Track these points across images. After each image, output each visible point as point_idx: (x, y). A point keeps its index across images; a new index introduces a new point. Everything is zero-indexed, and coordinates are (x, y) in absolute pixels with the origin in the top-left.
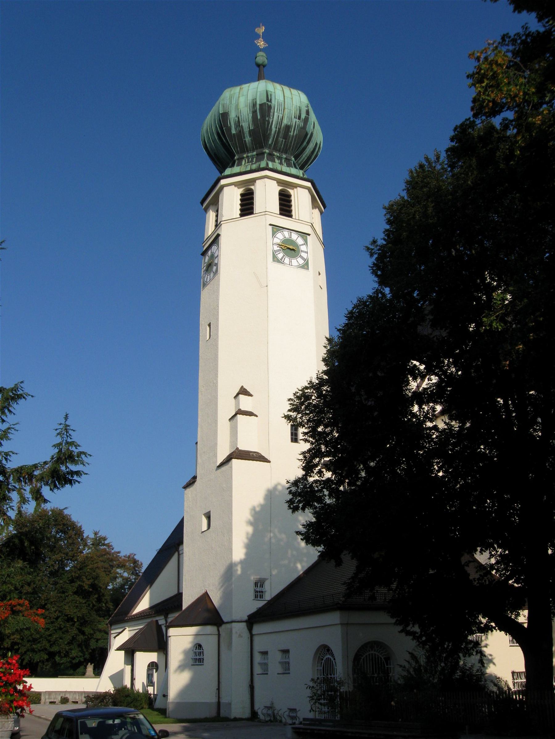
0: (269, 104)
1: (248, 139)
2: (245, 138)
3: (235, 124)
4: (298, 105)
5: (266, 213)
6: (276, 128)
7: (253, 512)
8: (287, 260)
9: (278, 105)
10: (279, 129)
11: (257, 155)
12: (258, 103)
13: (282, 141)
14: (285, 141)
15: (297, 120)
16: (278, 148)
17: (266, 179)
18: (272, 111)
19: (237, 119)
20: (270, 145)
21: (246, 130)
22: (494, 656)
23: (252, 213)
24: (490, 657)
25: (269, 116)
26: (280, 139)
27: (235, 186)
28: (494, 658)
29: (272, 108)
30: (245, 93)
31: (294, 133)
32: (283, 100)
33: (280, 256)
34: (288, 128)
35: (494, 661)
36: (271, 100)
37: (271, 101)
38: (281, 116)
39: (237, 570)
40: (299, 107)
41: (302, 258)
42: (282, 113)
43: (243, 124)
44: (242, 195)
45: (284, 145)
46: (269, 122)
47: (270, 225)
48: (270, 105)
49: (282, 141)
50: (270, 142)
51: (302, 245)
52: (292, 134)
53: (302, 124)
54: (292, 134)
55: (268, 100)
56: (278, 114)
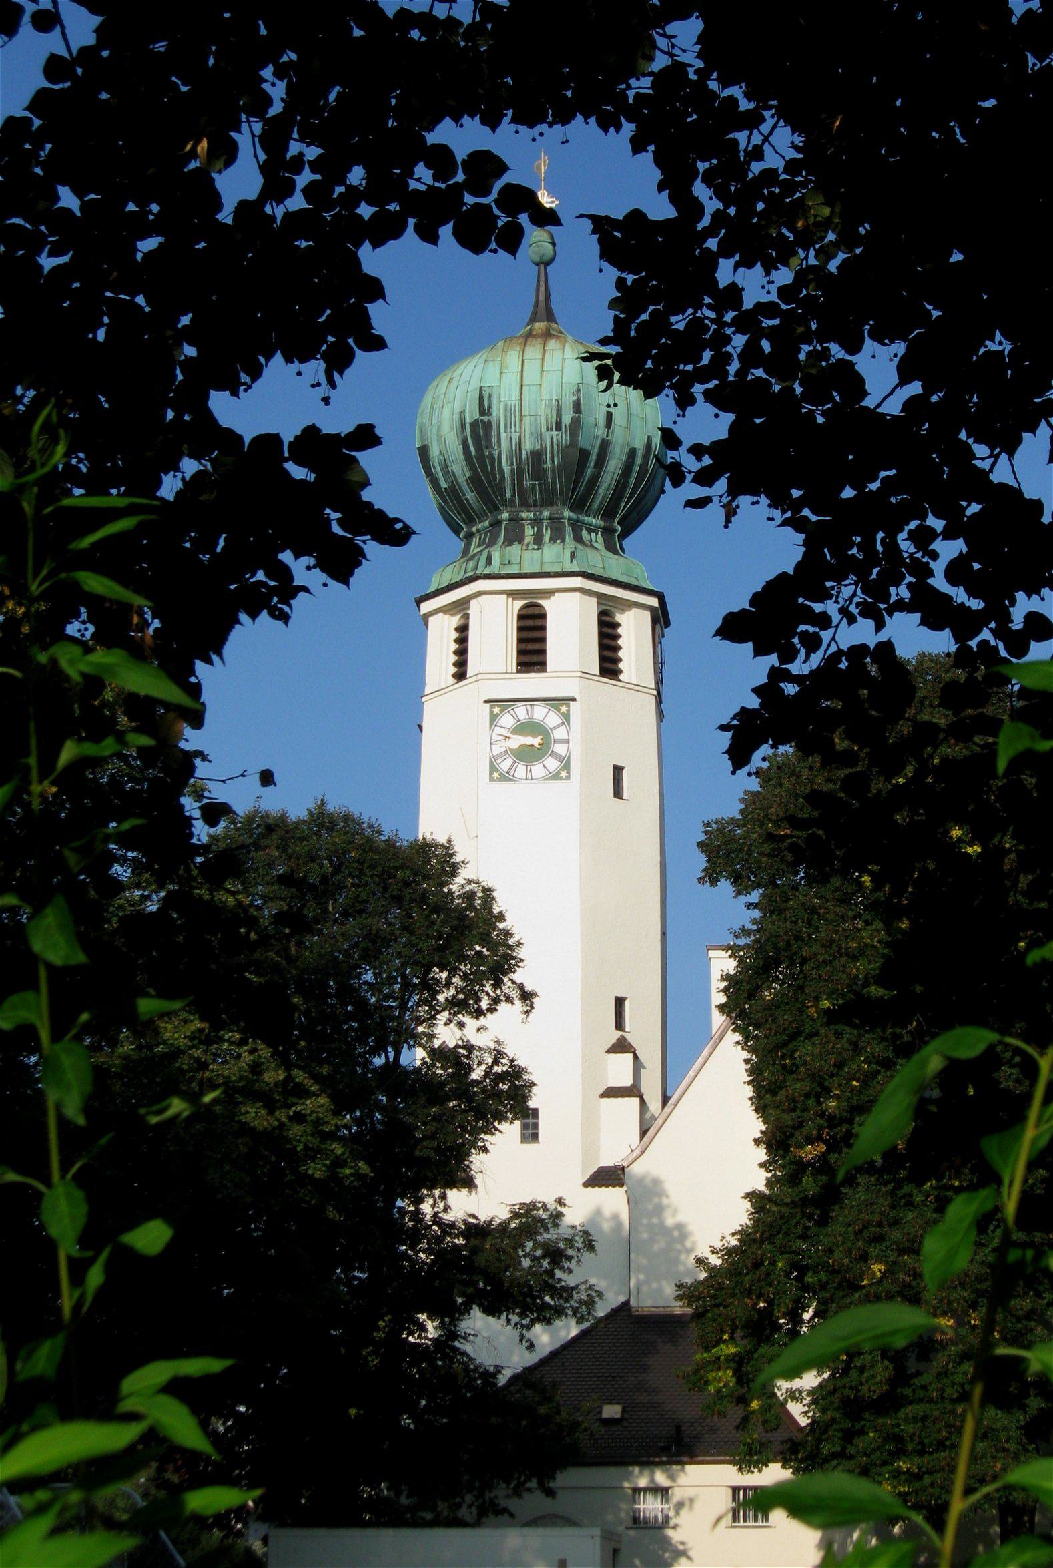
0: (486, 418)
1: (470, 496)
2: (464, 495)
3: (442, 469)
4: (554, 397)
5: (479, 677)
6: (512, 464)
8: (521, 770)
9: (506, 416)
11: (491, 525)
12: (468, 420)
13: (534, 485)
14: (540, 485)
15: (554, 433)
17: (484, 597)
18: (494, 432)
19: (442, 458)
20: (512, 500)
21: (462, 480)
22: (689, 1546)
23: (544, 670)
24: (681, 1547)
25: (489, 446)
26: (528, 483)
28: (691, 1549)
29: (495, 427)
30: (452, 399)
31: (553, 462)
32: (518, 397)
33: (505, 765)
34: (537, 456)
35: (690, 1553)
36: (489, 408)
37: (489, 413)
38: (515, 436)
40: (557, 400)
41: (555, 755)
42: (518, 429)
43: (454, 468)
44: (521, 617)
45: (540, 492)
46: (492, 457)
47: (486, 702)
48: (489, 422)
49: (534, 485)
50: (509, 495)
51: (558, 726)
52: (549, 464)
54: (549, 464)
55: (482, 412)
56: (509, 435)
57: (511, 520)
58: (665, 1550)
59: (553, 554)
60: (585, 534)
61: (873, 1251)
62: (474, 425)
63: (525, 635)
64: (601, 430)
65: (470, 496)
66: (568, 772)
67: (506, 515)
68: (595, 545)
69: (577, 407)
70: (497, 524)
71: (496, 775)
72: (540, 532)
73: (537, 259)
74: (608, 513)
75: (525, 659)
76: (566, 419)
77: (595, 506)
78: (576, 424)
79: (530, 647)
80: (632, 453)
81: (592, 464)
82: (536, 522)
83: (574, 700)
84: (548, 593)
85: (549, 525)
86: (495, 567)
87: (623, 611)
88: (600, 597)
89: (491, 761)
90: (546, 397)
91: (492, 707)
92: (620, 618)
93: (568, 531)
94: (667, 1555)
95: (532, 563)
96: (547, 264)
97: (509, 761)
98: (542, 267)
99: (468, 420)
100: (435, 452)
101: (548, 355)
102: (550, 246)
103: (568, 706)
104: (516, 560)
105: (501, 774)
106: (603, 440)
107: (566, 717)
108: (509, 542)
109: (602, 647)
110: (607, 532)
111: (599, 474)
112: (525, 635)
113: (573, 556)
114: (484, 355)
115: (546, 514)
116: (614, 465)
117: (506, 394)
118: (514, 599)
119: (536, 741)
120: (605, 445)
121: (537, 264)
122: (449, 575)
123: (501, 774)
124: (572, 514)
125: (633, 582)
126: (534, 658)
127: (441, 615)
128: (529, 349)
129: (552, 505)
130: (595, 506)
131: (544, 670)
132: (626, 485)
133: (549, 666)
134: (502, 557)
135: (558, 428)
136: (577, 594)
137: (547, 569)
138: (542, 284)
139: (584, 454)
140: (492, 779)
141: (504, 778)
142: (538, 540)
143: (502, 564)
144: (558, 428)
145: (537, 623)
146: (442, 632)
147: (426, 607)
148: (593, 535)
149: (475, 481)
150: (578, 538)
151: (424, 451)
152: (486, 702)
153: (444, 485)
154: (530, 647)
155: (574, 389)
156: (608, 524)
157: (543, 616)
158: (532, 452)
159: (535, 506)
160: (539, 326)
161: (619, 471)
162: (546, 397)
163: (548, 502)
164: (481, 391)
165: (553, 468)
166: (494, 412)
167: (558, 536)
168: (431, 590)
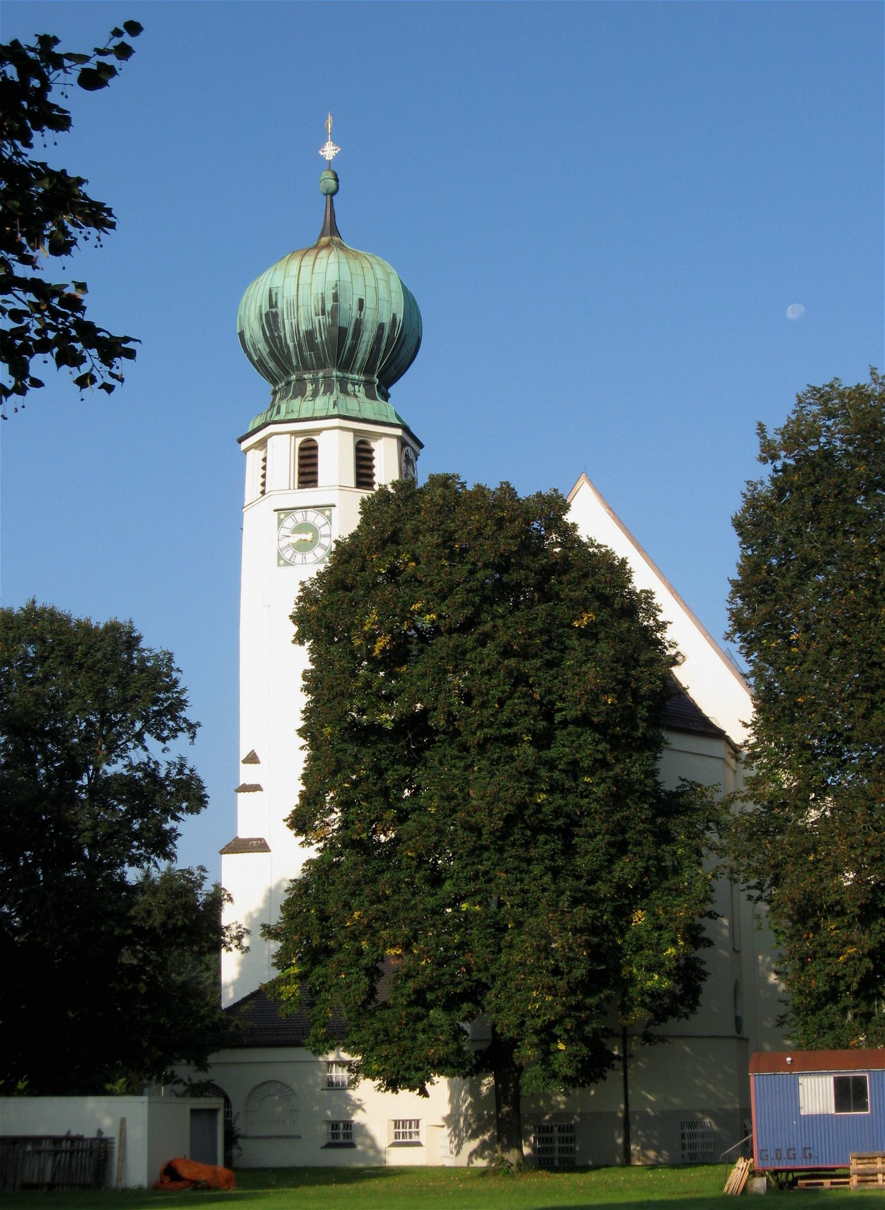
0: (274, 310)
7: (249, 920)
8: (299, 558)
10: (300, 345)
13: (311, 355)
15: (321, 317)
16: (310, 366)
17: (274, 437)
18: (280, 320)
20: (297, 366)
21: (264, 354)
23: (316, 486)
24: (358, 1103)
25: (277, 329)
26: (307, 354)
27: (256, 448)
33: (288, 555)
34: (310, 334)
35: (364, 1107)
36: (276, 302)
37: (276, 306)
38: (294, 321)
39: (228, 993)
44: (301, 449)
46: (280, 337)
47: (275, 511)
49: (311, 355)
51: (324, 525)
52: (319, 339)
53: (329, 320)
54: (319, 339)
55: (271, 306)
57: (297, 380)
58: (348, 1105)
59: (323, 403)
60: (350, 387)
61: (354, 902)
62: (267, 315)
63: (312, 461)
64: (355, 313)
65: (271, 364)
66: (284, 565)
67: (294, 377)
68: (358, 394)
69: (336, 297)
70: (288, 384)
71: (282, 562)
72: (317, 386)
73: (325, 192)
74: (368, 369)
75: (304, 478)
76: (329, 307)
77: (358, 365)
78: (335, 310)
79: (307, 470)
80: (381, 327)
81: (350, 338)
82: (315, 381)
83: (334, 506)
84: (318, 431)
85: (324, 382)
86: (281, 416)
87: (376, 440)
88: (356, 432)
89: (279, 554)
90: (314, 291)
91: (279, 514)
92: (374, 445)
93: (337, 386)
94: (348, 1108)
95: (307, 411)
96: (333, 194)
97: (291, 552)
98: (329, 196)
99: (264, 312)
100: (247, 336)
101: (318, 261)
102: (333, 182)
103: (330, 510)
104: (296, 409)
105: (285, 561)
106: (357, 319)
107: (329, 518)
108: (295, 396)
109: (358, 466)
110: (368, 384)
111: (356, 344)
112: (305, 461)
113: (335, 404)
114: (271, 270)
115: (321, 374)
116: (368, 336)
117: (287, 293)
118: (296, 437)
119: (309, 537)
120: (359, 323)
121: (326, 195)
122: (258, 422)
123: (285, 561)
124: (339, 373)
125: (384, 419)
126: (309, 478)
127: (253, 450)
128: (306, 258)
129: (325, 368)
130: (358, 365)
131: (316, 486)
132: (379, 349)
133: (320, 483)
134: (287, 408)
135: (323, 313)
136: (337, 431)
137: (317, 414)
138: (329, 209)
139: (343, 331)
140: (279, 565)
141: (288, 564)
142: (315, 394)
143: (287, 413)
144: (323, 313)
145: (312, 452)
146: (254, 459)
147: (245, 445)
148: (357, 387)
149: (272, 354)
150: (344, 391)
151: (242, 335)
152: (275, 511)
153: (256, 358)
154: (307, 470)
155: (333, 285)
156: (368, 378)
157: (316, 448)
158: (306, 332)
159: (314, 369)
160: (325, 239)
161: (371, 340)
162: (314, 291)
163: (322, 366)
164: (270, 291)
165: (322, 341)
166: (279, 305)
167: (329, 389)
168: (250, 429)
